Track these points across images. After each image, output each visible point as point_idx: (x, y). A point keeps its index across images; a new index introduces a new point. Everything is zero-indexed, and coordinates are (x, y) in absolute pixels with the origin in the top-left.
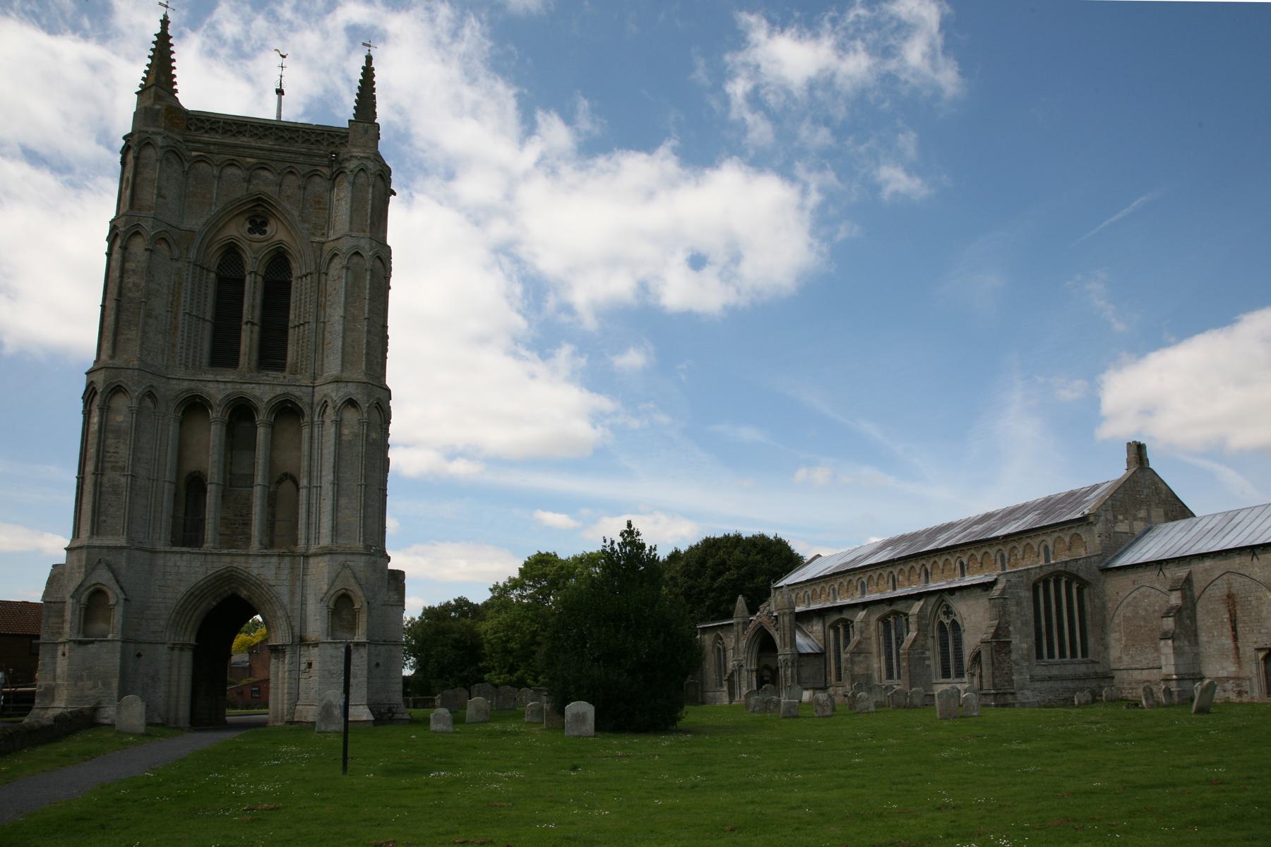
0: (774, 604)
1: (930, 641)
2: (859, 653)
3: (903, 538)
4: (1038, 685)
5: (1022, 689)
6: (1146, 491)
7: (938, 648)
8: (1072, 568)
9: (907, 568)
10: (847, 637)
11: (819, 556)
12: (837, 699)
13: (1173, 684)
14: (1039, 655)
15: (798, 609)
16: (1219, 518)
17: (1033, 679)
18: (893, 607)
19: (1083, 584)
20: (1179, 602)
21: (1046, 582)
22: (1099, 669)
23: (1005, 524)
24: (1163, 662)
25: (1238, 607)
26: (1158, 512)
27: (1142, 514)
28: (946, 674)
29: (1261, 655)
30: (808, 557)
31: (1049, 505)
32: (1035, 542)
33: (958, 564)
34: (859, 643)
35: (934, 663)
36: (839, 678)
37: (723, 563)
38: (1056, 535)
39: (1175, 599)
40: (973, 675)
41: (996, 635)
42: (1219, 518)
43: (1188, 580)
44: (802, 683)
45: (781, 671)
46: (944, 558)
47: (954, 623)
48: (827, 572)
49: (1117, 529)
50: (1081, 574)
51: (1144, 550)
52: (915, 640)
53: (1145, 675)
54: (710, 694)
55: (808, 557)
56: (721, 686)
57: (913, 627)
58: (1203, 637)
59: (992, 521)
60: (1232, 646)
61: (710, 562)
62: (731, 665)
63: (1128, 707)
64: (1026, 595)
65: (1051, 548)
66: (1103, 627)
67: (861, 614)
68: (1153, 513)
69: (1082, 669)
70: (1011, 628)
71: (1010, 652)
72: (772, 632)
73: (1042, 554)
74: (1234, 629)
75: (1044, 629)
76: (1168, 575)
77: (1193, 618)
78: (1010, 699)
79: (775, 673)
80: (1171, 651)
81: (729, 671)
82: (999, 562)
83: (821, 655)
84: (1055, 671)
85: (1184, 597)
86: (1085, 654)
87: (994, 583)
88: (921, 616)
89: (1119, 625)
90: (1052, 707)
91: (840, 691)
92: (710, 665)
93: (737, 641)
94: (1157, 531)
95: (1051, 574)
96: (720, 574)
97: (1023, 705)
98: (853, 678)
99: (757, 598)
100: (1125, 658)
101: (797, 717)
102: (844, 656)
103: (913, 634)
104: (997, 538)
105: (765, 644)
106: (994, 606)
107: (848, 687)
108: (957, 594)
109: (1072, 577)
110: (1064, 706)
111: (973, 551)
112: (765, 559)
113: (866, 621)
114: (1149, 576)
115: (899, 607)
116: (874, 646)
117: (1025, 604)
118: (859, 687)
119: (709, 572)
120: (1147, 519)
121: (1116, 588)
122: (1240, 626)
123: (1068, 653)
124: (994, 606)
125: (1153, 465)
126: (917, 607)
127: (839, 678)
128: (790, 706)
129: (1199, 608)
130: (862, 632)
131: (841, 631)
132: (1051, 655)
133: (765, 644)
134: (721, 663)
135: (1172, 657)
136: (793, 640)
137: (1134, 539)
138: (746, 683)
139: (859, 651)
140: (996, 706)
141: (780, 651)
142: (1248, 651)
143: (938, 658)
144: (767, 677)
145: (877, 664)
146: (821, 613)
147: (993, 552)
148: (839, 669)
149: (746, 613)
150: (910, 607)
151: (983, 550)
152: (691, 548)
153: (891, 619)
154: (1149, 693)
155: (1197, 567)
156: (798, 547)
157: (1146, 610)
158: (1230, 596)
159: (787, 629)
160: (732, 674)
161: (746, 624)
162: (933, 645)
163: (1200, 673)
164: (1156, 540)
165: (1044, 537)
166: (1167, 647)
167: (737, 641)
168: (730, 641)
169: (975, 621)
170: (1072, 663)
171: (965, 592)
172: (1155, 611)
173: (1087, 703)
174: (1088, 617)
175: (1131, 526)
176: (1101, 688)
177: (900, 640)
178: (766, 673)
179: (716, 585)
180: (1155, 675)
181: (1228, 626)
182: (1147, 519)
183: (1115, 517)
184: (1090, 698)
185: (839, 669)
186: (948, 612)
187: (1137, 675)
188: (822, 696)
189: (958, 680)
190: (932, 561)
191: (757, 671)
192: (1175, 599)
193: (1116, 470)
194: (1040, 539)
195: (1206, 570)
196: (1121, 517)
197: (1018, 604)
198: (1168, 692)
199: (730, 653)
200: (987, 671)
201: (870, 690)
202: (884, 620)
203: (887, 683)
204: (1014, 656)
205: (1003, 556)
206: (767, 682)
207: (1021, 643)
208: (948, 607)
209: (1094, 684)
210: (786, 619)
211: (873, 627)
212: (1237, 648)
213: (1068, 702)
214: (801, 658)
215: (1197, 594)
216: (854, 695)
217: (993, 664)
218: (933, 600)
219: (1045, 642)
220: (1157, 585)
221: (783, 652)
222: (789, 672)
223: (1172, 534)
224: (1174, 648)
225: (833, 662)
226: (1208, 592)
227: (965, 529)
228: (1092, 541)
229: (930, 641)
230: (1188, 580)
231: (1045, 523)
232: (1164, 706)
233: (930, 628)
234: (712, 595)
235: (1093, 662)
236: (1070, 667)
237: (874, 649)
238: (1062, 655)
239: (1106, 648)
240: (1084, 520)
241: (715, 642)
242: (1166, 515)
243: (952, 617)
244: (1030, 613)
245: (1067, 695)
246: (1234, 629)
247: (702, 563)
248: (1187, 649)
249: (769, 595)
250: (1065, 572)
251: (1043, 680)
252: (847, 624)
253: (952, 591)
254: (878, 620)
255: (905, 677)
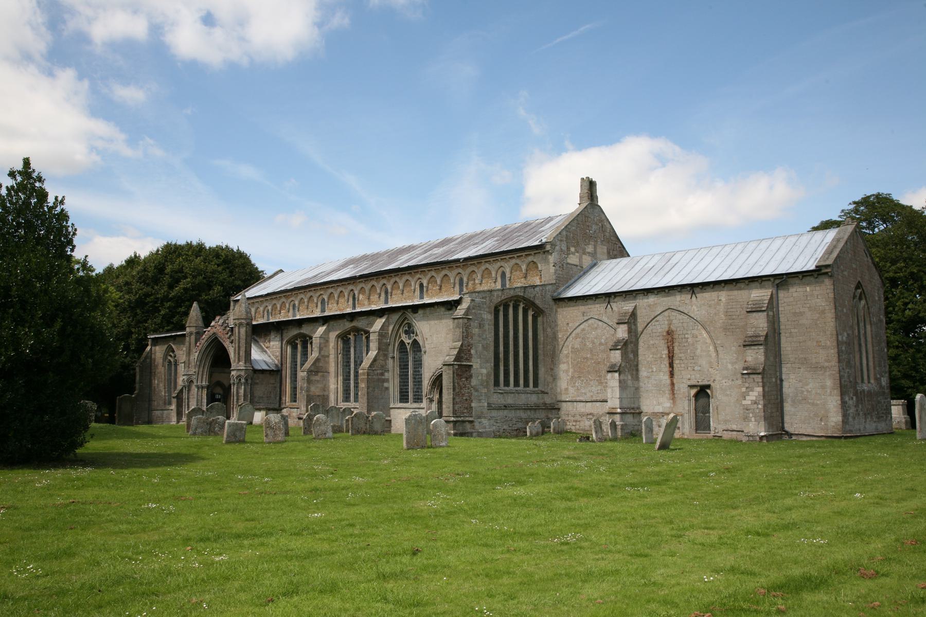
0: (235, 314)
1: (390, 361)
2: (317, 373)
3: (365, 258)
4: (494, 413)
5: (479, 417)
6: (594, 227)
7: (397, 370)
8: (530, 294)
9: (367, 287)
10: (305, 355)
11: (281, 271)
12: (292, 422)
13: (617, 418)
14: (497, 383)
15: (254, 323)
16: (657, 258)
17: (490, 407)
18: (355, 324)
19: (539, 312)
20: (626, 335)
21: (506, 307)
22: (548, 400)
23: (465, 248)
24: (609, 395)
25: (676, 344)
26: (602, 249)
27: (590, 249)
28: (404, 398)
29: (693, 392)
30: (268, 273)
31: (506, 233)
32: (493, 267)
33: (418, 286)
34: (317, 360)
35: (393, 386)
36: (294, 399)
37: (181, 270)
38: (514, 261)
39: (622, 332)
40: (431, 400)
41: (458, 358)
42: (657, 258)
43: (633, 315)
44: (255, 403)
45: (234, 389)
46: (405, 278)
47: (415, 343)
48: (289, 287)
49: (569, 261)
50: (537, 302)
51: (593, 283)
52: (375, 360)
53: (589, 408)
54: (158, 413)
55: (268, 273)
56: (170, 404)
57: (374, 346)
58: (643, 373)
59: (451, 245)
60: (668, 381)
61: (168, 269)
62: (181, 380)
63: (581, 440)
64: (488, 317)
65: (508, 275)
66: (554, 357)
67: (321, 330)
68: (599, 250)
69: (533, 399)
70: (473, 352)
71: (471, 376)
72: (227, 344)
73: (499, 279)
74: (671, 365)
75: (501, 356)
76: (615, 308)
77: (636, 354)
78: (468, 427)
79: (227, 390)
80: (617, 384)
81: (179, 388)
82: (457, 286)
83: (275, 373)
84: (510, 400)
85: (630, 331)
86: (536, 384)
87: (458, 302)
88: (382, 334)
89: (567, 356)
90: (500, 437)
91: (295, 413)
92: (159, 385)
93: (189, 353)
94: (602, 267)
95: (511, 299)
96: (177, 281)
97: (480, 435)
98: (309, 400)
99: (215, 308)
100: (571, 390)
101: (244, 442)
102: (301, 374)
103: (373, 353)
104: (457, 261)
105: (218, 358)
106: (457, 327)
107: (303, 409)
108: (420, 312)
109: (530, 304)
110: (516, 436)
111: (433, 273)
112: (228, 272)
113: (325, 338)
114: (597, 309)
115: (360, 323)
116: (333, 365)
117: (487, 327)
118: (316, 409)
119: (167, 279)
120: (593, 255)
121: (567, 317)
122: (676, 362)
123: (522, 382)
124: (457, 327)
125: (601, 203)
126: (379, 323)
127: (294, 399)
128: (236, 428)
129: (641, 344)
130: (320, 349)
131: (299, 347)
132: (507, 383)
133: (218, 358)
134: (171, 381)
135: (617, 390)
136: (248, 353)
137: (582, 272)
138: (196, 399)
139: (318, 370)
140: (455, 435)
141: (234, 365)
142: (682, 387)
143: (397, 380)
144: (219, 394)
145: (334, 385)
146: (279, 327)
147: (452, 274)
148: (294, 389)
149: (201, 323)
150: (372, 324)
151: (443, 273)
152: (152, 254)
153: (352, 337)
154: (598, 425)
155: (643, 303)
156: (259, 262)
157: (593, 343)
158: (670, 333)
159: (243, 342)
160: (181, 391)
161: (199, 335)
162: (393, 366)
163: (639, 408)
164: (602, 275)
165: (502, 263)
166: (613, 380)
167: (189, 353)
168: (181, 353)
169: (438, 341)
170: (534, 392)
171: (428, 310)
172: (601, 344)
173: (537, 434)
174: (540, 346)
175: (580, 259)
176: (549, 419)
177: (358, 363)
178: (219, 390)
179: (172, 294)
180: (599, 409)
181: (666, 362)
182: (593, 255)
183: (568, 249)
184: (540, 430)
185: (294, 389)
186: (410, 331)
187: (582, 408)
188: (274, 417)
189: (416, 405)
190: (392, 281)
191: (208, 387)
192: (622, 332)
193: (572, 204)
194: (499, 264)
195: (649, 306)
196: (573, 249)
197: (481, 326)
198: (613, 425)
199: (181, 369)
200: (447, 396)
201: (327, 412)
202: (344, 338)
203: (343, 405)
204: (474, 382)
205: (461, 281)
206: (219, 400)
207: (481, 368)
208: (410, 325)
209: (542, 415)
210: (243, 330)
211: (332, 344)
212: (673, 384)
213: (520, 433)
214: (256, 374)
215: (640, 329)
216: (310, 418)
217: (454, 389)
218: (395, 317)
219: (502, 368)
220: (605, 319)
221: (237, 366)
222: (242, 391)
223: (616, 270)
224: (620, 382)
225: (288, 380)
226: (650, 327)
227: (426, 252)
228: (547, 272)
229: (390, 361)
230: (633, 315)
231: (504, 248)
232: (610, 440)
233: (391, 348)
234: (168, 304)
235: (543, 392)
236: (523, 396)
237: (332, 368)
238: (517, 384)
239: (555, 378)
240: (540, 248)
241: (165, 358)
242: (609, 253)
243: (413, 337)
244: (490, 337)
245: (520, 425)
246: (671, 365)
247: (160, 269)
248: (630, 383)
249: (227, 308)
250: (524, 298)
251: (499, 409)
252: (306, 340)
253: (415, 308)
254: (338, 336)
255: (363, 399)
